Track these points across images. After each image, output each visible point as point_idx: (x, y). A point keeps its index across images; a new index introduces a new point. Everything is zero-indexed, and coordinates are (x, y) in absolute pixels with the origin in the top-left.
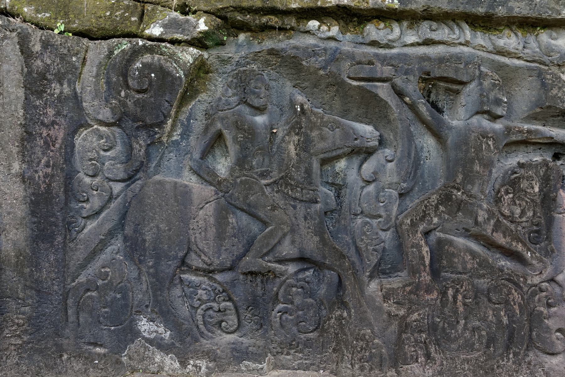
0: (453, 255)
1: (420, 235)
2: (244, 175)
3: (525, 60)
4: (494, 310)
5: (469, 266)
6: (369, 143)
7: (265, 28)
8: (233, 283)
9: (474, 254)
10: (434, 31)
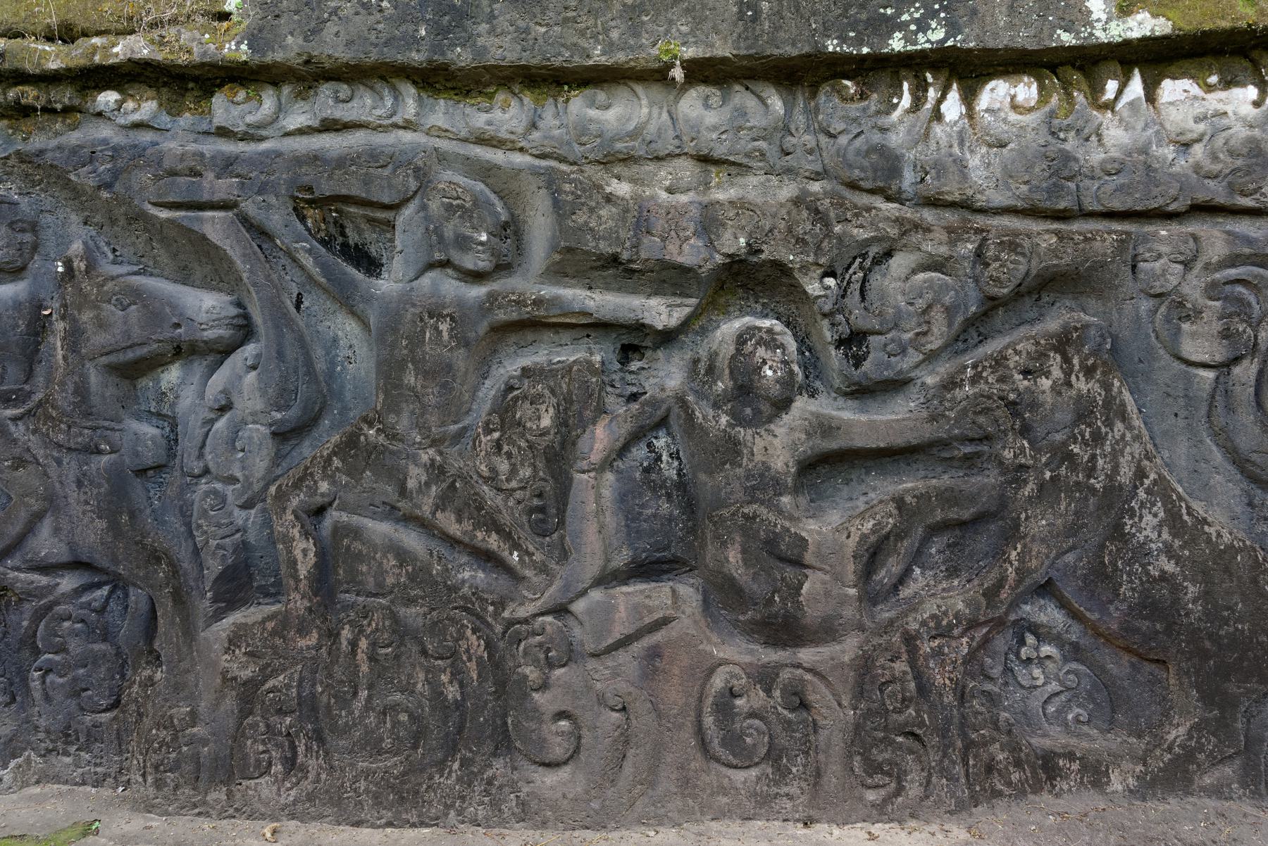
0: (359, 557)
1: (292, 517)
4: (428, 672)
5: (390, 580)
6: (205, 333)
9: (403, 556)
10: (344, 101)
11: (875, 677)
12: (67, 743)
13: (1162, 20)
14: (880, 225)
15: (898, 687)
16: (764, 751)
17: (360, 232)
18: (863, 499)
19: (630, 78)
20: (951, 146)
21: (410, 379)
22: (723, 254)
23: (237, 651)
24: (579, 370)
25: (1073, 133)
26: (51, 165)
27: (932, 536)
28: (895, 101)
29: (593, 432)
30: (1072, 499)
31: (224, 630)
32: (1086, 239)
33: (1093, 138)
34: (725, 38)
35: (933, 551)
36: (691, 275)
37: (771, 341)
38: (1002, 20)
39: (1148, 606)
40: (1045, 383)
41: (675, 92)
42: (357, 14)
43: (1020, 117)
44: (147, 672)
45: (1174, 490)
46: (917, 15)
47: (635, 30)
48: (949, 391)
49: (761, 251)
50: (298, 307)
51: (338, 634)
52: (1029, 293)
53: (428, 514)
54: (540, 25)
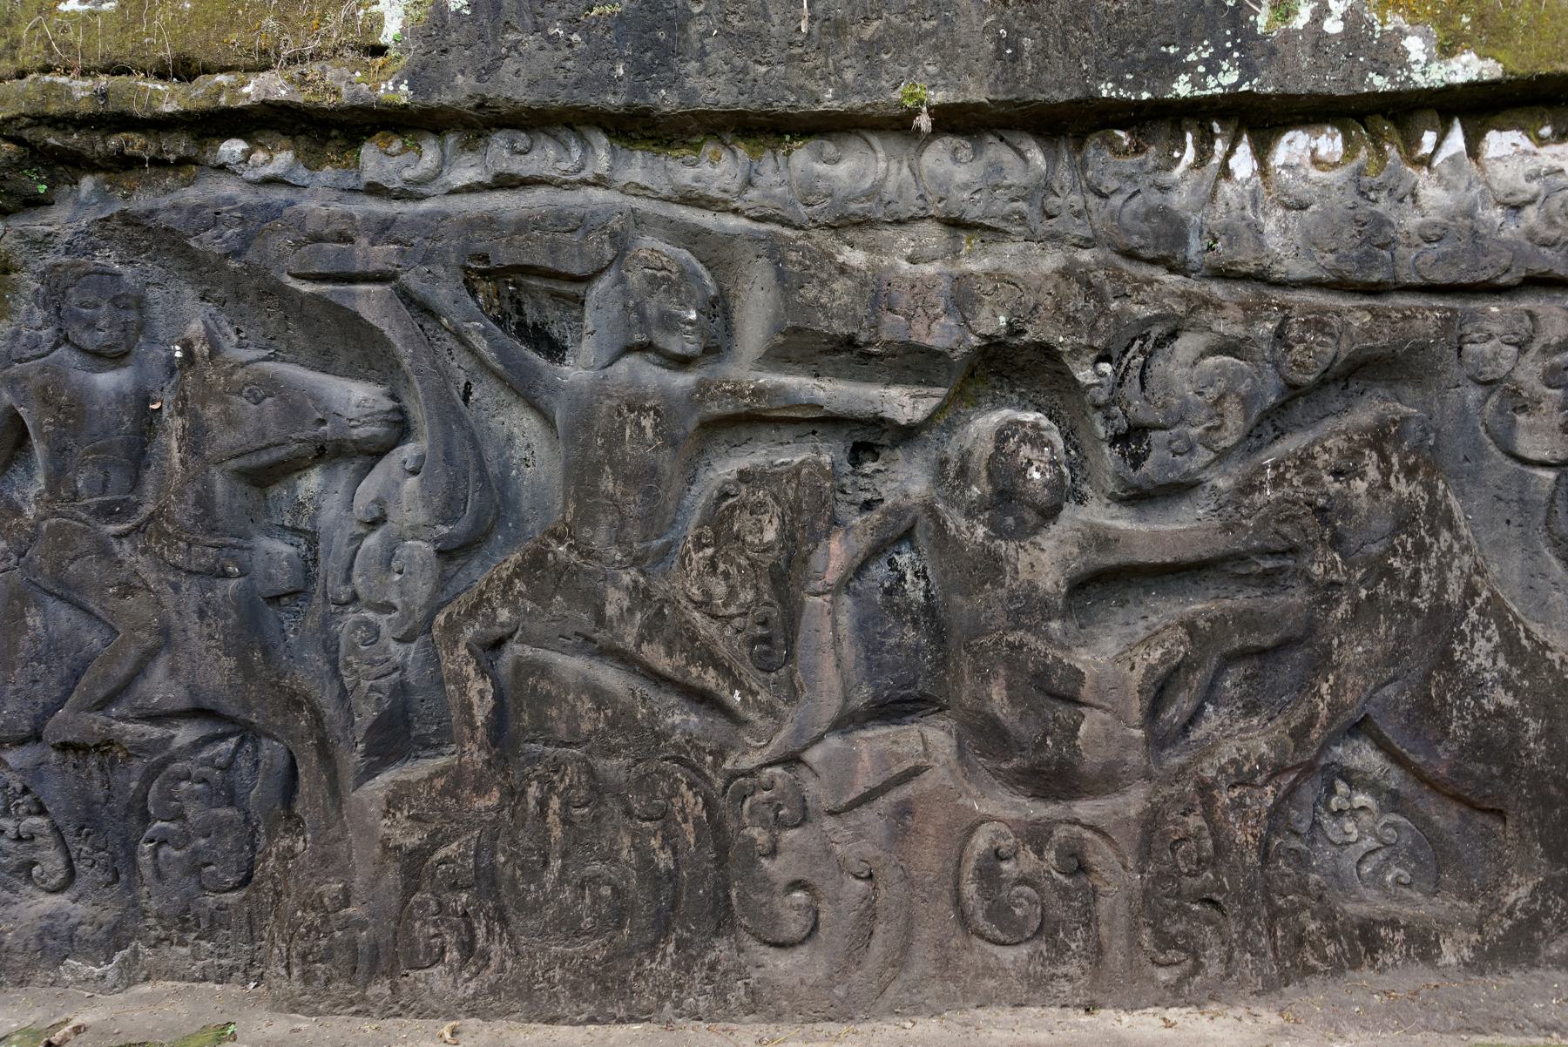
0: (547, 699)
1: (465, 652)
2: (55, 514)
3: (748, 217)
4: (634, 836)
5: (586, 727)
6: (355, 431)
7: (124, 163)
8: (37, 768)
9: (600, 697)
10: (522, 153)
11: (1165, 834)
12: (183, 930)
13: (1491, 62)
14: (1166, 301)
15: (1193, 845)
16: (1036, 924)
17: (540, 309)
18: (1142, 623)
19: (864, 128)
20: (1243, 208)
21: (608, 484)
22: (980, 336)
23: (398, 815)
24: (810, 474)
25: (1385, 193)
26: (166, 229)
27: (1226, 666)
28: (1176, 154)
29: (827, 547)
30: (1393, 621)
31: (380, 789)
32: (1405, 317)
33: (1408, 199)
34: (980, 81)
35: (1228, 684)
36: (940, 360)
37: (1036, 439)
38: (1306, 62)
39: (1482, 746)
40: (1360, 486)
41: (916, 144)
42: (541, 49)
43: (1322, 174)
44: (286, 842)
45: (1509, 610)
46: (1205, 55)
47: (873, 71)
48: (1247, 495)
49: (1024, 332)
50: (466, 400)
51: (524, 792)
52: (1335, 380)
53: (631, 647)
54: (760, 63)
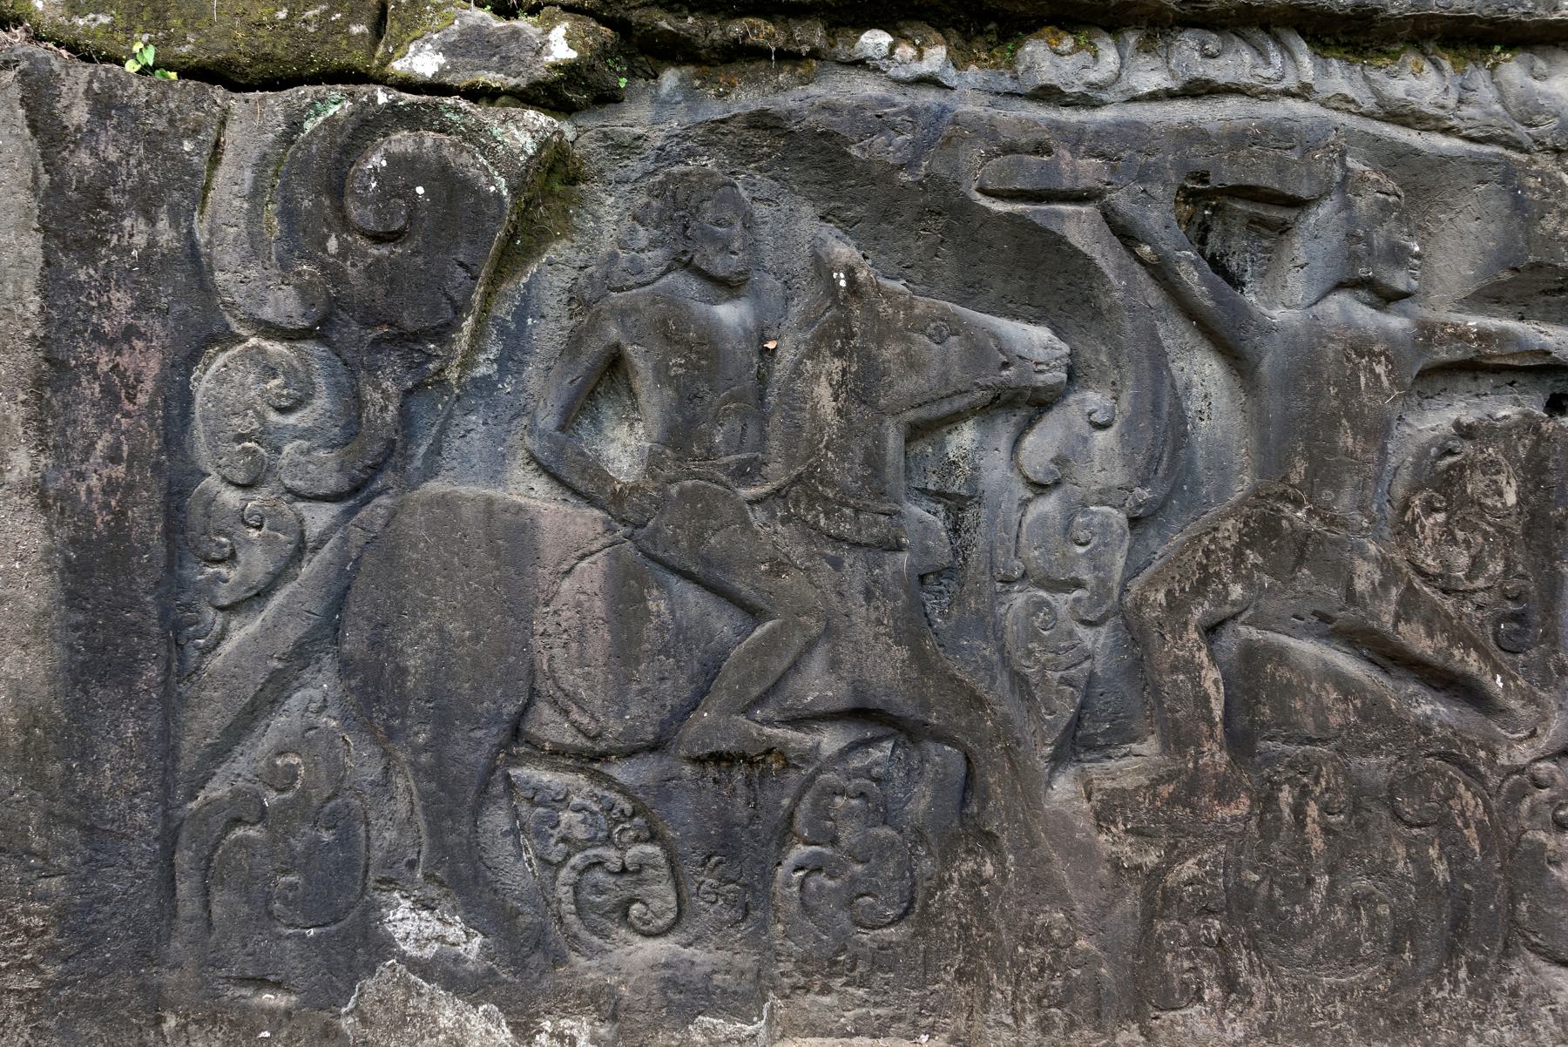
0: (1288, 689)
2: (691, 475)
4: (1408, 845)
5: (1335, 720)
6: (1041, 377)
8: (664, 789)
10: (1213, 56)
12: (831, 975)
21: (1347, 440)
